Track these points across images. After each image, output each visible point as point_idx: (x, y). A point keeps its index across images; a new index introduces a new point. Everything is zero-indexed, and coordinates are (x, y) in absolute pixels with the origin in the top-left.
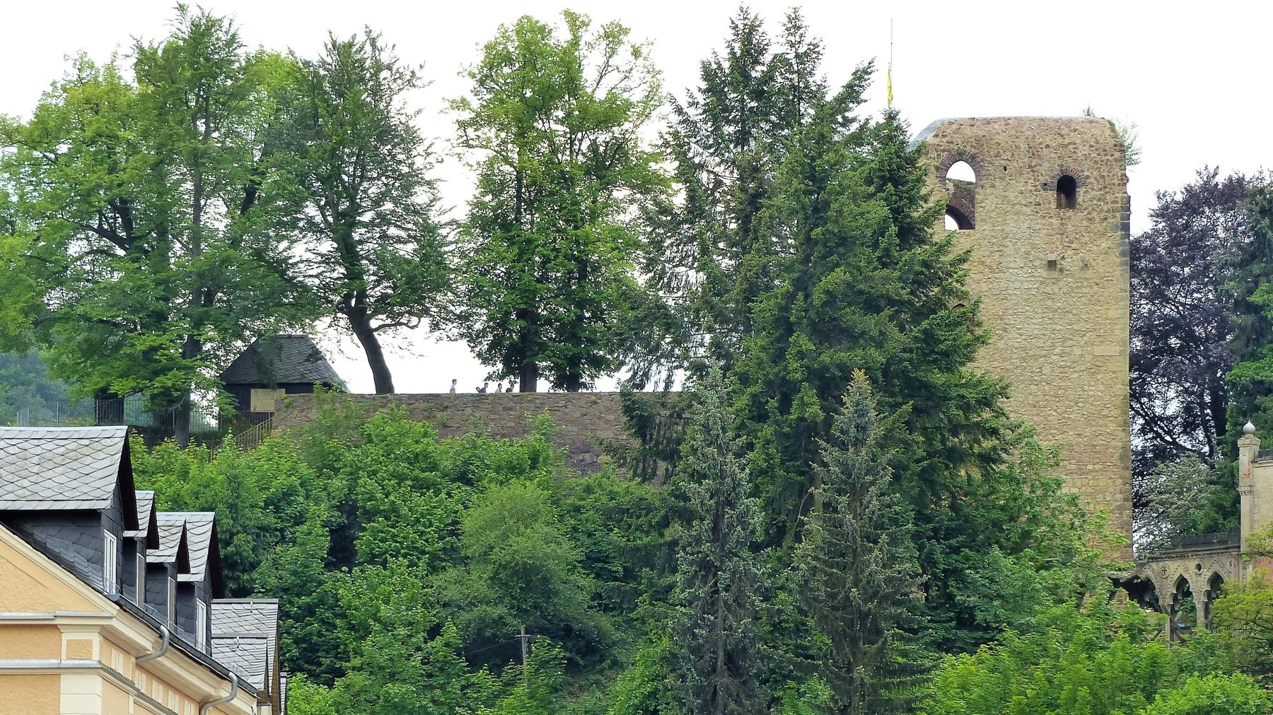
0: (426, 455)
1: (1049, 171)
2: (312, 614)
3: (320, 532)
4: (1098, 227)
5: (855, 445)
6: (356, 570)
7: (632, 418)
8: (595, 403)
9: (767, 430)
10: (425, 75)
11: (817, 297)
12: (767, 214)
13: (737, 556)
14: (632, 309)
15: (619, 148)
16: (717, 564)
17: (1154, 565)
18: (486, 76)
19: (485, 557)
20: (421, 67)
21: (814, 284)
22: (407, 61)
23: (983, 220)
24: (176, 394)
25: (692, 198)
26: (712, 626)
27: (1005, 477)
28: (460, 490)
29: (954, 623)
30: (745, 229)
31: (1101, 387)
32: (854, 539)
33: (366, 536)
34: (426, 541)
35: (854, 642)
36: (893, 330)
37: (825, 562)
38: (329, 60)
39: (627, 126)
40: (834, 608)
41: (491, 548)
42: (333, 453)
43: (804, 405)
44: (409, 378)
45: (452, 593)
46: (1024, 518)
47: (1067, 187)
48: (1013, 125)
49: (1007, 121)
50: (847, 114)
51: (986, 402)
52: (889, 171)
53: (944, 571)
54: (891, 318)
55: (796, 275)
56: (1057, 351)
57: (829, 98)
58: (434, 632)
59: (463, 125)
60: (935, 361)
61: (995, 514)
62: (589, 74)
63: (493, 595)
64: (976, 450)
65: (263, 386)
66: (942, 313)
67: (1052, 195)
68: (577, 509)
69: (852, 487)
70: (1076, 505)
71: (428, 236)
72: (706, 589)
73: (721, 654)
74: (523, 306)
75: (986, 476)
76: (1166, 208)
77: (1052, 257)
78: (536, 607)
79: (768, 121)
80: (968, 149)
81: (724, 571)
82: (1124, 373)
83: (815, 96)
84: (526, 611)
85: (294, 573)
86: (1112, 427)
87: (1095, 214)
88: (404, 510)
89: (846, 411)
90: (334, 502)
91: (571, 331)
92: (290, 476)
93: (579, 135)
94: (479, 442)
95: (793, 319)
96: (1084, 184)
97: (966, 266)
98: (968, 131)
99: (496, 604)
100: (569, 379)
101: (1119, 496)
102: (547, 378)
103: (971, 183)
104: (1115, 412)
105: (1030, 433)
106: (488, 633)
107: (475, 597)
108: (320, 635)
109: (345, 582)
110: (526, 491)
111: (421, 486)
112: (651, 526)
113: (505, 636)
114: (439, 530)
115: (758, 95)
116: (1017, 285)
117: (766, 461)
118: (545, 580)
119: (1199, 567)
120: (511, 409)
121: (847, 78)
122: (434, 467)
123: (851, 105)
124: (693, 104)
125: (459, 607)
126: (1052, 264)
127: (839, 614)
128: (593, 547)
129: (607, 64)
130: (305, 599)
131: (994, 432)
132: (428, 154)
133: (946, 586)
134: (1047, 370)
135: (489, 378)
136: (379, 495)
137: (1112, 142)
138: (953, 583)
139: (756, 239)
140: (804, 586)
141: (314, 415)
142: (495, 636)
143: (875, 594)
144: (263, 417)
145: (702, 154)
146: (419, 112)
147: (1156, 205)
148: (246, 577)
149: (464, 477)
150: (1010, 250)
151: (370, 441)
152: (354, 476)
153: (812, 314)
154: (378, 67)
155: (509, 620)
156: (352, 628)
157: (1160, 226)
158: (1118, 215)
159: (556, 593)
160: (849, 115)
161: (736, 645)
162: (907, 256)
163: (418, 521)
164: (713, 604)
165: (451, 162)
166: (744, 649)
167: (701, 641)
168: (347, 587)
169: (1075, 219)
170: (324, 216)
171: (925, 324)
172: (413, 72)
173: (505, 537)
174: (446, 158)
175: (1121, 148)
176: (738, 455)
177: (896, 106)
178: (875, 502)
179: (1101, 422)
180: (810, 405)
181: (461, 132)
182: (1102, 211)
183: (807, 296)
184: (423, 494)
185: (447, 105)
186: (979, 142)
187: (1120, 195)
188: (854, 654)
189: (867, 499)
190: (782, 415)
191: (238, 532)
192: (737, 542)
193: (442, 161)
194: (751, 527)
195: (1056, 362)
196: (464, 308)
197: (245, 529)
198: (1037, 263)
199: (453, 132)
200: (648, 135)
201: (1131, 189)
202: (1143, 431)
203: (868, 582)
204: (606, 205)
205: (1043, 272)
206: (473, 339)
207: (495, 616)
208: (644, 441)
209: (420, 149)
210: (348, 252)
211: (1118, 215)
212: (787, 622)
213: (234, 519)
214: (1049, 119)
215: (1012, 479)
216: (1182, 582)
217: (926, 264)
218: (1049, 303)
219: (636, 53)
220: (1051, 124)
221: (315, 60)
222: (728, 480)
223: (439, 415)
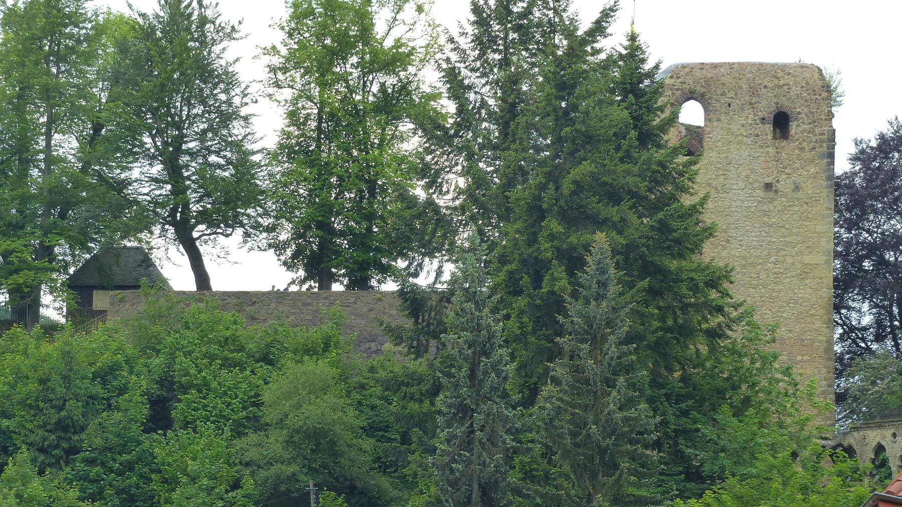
0: (235, 338)
1: (767, 107)
2: (131, 469)
3: (140, 399)
4: (808, 155)
5: (596, 300)
6: (170, 433)
7: (406, 300)
8: (380, 300)
9: (521, 302)
10: (243, 30)
11: (567, 186)
12: (524, 120)
13: (491, 400)
14: (408, 208)
15: (404, 89)
16: (473, 407)
17: (855, 434)
18: (293, 29)
19: (281, 424)
20: (240, 23)
21: (564, 177)
22: (227, 15)
23: (711, 149)
24: (26, 290)
25: (460, 111)
26: (468, 462)
27: (729, 350)
28: (262, 369)
29: (683, 477)
30: (504, 133)
31: (810, 291)
32: (595, 382)
33: (181, 406)
34: (232, 410)
35: (594, 475)
36: (632, 217)
37: (568, 403)
38: (162, 14)
39: (411, 69)
40: (577, 445)
41: (286, 416)
42: (155, 337)
43: (554, 279)
44: (222, 280)
45: (252, 454)
46: (744, 387)
47: (781, 122)
49: (731, 65)
50: (595, 45)
51: (713, 284)
52: (631, 84)
53: (675, 431)
54: (631, 208)
55: (548, 169)
56: (772, 259)
57: (580, 33)
58: (236, 485)
59: (273, 70)
60: (669, 247)
61: (719, 383)
62: (380, 28)
63: (287, 456)
64: (705, 326)
65: (103, 288)
66: (675, 205)
67: (769, 128)
68: (363, 387)
69: (594, 337)
70: (789, 375)
71: (243, 165)
72: (463, 429)
73: (476, 487)
74: (320, 218)
75: (713, 350)
76: (862, 152)
77: (768, 180)
78: (324, 466)
79: (527, 50)
80: (698, 88)
81: (479, 413)
82: (827, 292)
83: (569, 32)
84: (316, 470)
85: (118, 435)
86: (818, 324)
87: (805, 144)
88: (214, 385)
89: (588, 270)
90: (156, 377)
91: (361, 241)
92: (116, 354)
93: (371, 78)
94: (280, 329)
95: (545, 206)
96: (796, 119)
97: (695, 168)
98: (698, 74)
99: (290, 464)
100: (359, 282)
101: (824, 383)
102: (342, 283)
103: (700, 127)
104: (821, 312)
105: (749, 313)
106: (283, 488)
107: (272, 458)
108: (138, 487)
109: (160, 443)
110: (321, 368)
111: (228, 364)
112: (422, 394)
113: (297, 490)
114: (243, 401)
115: (518, 28)
116: (738, 203)
117: (519, 328)
118: (332, 443)
119: (894, 435)
120: (309, 304)
121: (597, 15)
122: (241, 349)
123: (599, 38)
124: (464, 34)
125: (259, 467)
126: (768, 186)
127: (580, 451)
128: (375, 418)
129: (395, 19)
130: (125, 457)
131: (720, 309)
132: (246, 95)
133: (677, 444)
134: (763, 276)
135: (293, 282)
136: (193, 372)
137: (820, 83)
138: (683, 442)
139: (514, 141)
140: (550, 424)
141: (142, 307)
142: (289, 491)
143: (613, 432)
144: (102, 313)
145: (470, 78)
146: (237, 60)
147: (853, 150)
148: (76, 438)
149: (267, 359)
150: (733, 174)
151: (188, 328)
152: (172, 357)
153: (562, 203)
154: (203, 21)
155: (303, 478)
156: (165, 481)
157: (857, 168)
158: (825, 145)
159: (342, 455)
160: (597, 46)
161: (490, 479)
162: (645, 155)
163: (225, 393)
164: (469, 443)
165: (264, 102)
166: (496, 482)
167: (457, 474)
168: (161, 447)
169: (788, 148)
170: (155, 142)
171: (660, 215)
172: (233, 27)
173: (298, 406)
174: (259, 99)
175: (827, 88)
176: (495, 310)
177: (637, 31)
178: (613, 349)
179: (809, 320)
180: (558, 279)
181: (272, 75)
182: (811, 141)
183: (557, 188)
184: (231, 372)
185: (260, 51)
186: (708, 82)
187: (827, 128)
188: (594, 486)
189: (606, 346)
190: (534, 289)
191: (70, 399)
192: (491, 387)
193: (256, 102)
194: (504, 374)
195: (772, 265)
196: (271, 220)
197: (77, 397)
198: (756, 185)
199: (265, 75)
200: (429, 78)
201: (835, 123)
202: (842, 338)
203: (607, 421)
204: (393, 137)
205: (760, 193)
206: (278, 247)
207: (289, 473)
208: (416, 322)
209: (238, 90)
210: (174, 172)
211: (825, 145)
212: (537, 471)
213: (67, 388)
214: (767, 64)
215: (734, 352)
216: (880, 449)
217: (662, 164)
218: (765, 219)
219: (420, 9)
220: (769, 68)
221: (150, 13)
222: (484, 332)
223: (248, 309)
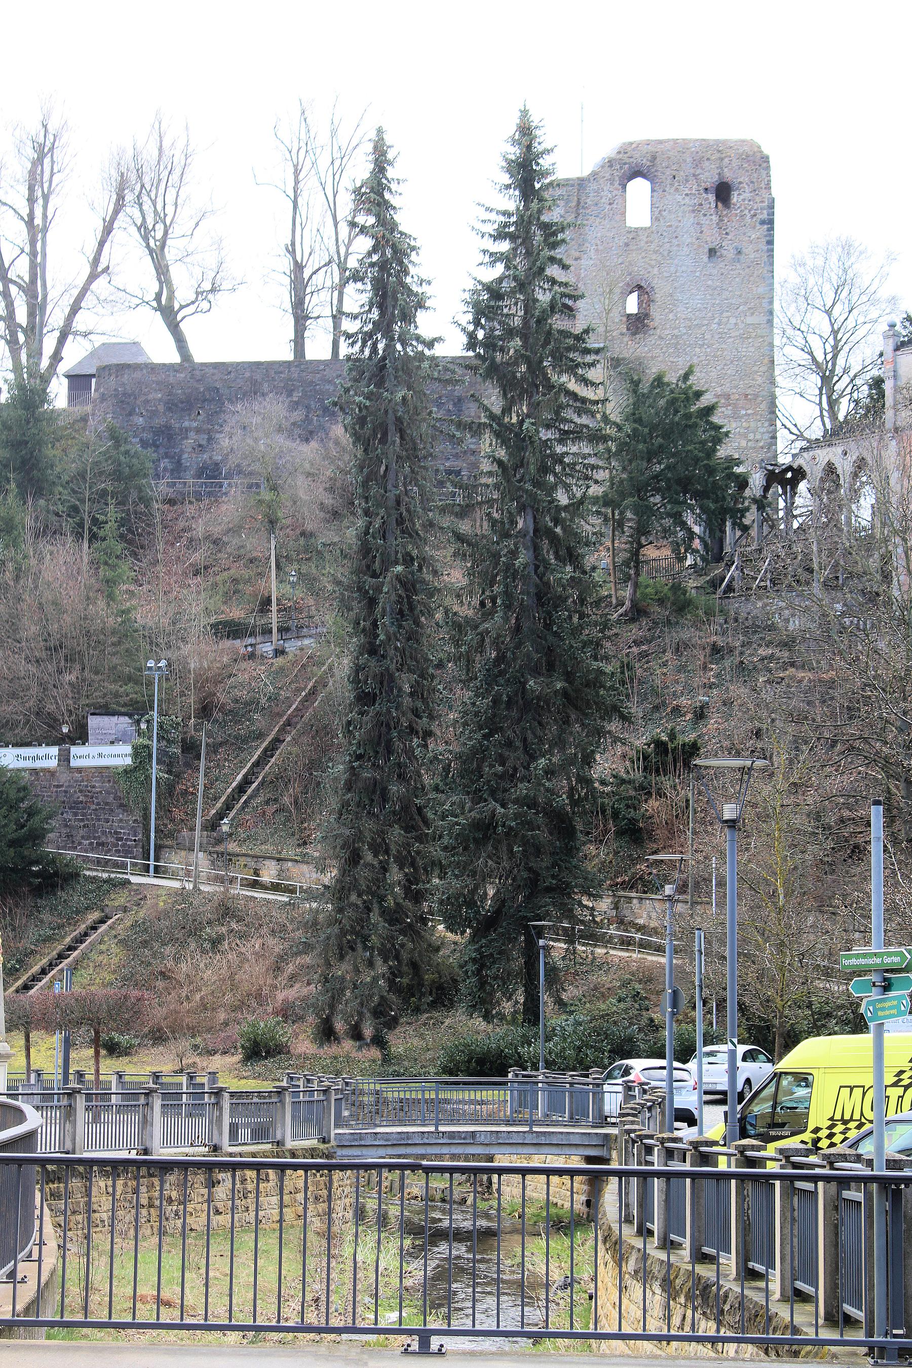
1: (710, 177)
17: (805, 454)
48: (681, 146)
49: (675, 141)
67: (712, 197)
98: (645, 149)
116: (684, 268)
216: (830, 469)
